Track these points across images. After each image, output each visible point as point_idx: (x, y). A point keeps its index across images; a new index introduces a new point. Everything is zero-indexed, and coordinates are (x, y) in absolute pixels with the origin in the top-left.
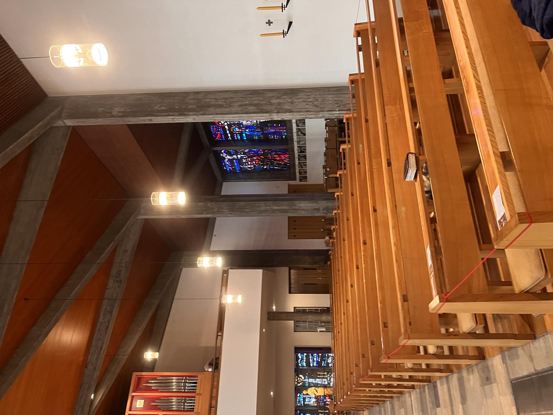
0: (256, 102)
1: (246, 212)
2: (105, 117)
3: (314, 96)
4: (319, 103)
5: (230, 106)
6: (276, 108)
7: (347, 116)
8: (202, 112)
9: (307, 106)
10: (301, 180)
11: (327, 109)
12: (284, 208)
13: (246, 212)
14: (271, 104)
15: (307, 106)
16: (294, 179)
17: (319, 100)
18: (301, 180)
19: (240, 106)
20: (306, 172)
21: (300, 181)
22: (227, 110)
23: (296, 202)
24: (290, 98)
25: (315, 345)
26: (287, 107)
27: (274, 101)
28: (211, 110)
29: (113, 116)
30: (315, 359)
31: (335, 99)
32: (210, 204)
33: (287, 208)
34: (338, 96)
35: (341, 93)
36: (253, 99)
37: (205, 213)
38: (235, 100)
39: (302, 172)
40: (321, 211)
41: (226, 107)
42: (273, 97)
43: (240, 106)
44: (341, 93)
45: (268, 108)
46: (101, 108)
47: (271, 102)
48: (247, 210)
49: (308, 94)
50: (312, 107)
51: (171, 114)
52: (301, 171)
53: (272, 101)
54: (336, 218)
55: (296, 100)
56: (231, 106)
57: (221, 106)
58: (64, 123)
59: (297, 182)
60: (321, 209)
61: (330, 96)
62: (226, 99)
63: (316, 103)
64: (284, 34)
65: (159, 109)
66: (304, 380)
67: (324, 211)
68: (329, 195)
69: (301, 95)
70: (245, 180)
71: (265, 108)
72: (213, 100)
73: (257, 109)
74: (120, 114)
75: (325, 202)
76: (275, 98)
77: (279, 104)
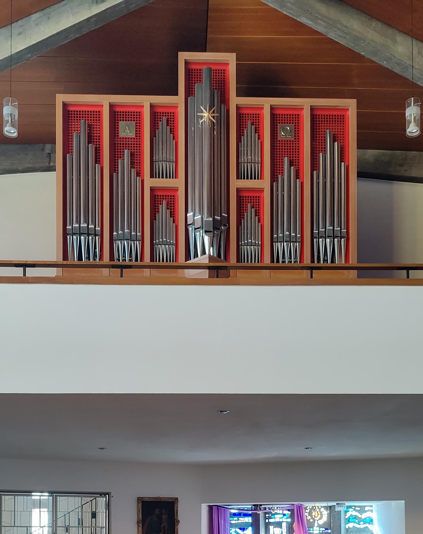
66: (316, 525)
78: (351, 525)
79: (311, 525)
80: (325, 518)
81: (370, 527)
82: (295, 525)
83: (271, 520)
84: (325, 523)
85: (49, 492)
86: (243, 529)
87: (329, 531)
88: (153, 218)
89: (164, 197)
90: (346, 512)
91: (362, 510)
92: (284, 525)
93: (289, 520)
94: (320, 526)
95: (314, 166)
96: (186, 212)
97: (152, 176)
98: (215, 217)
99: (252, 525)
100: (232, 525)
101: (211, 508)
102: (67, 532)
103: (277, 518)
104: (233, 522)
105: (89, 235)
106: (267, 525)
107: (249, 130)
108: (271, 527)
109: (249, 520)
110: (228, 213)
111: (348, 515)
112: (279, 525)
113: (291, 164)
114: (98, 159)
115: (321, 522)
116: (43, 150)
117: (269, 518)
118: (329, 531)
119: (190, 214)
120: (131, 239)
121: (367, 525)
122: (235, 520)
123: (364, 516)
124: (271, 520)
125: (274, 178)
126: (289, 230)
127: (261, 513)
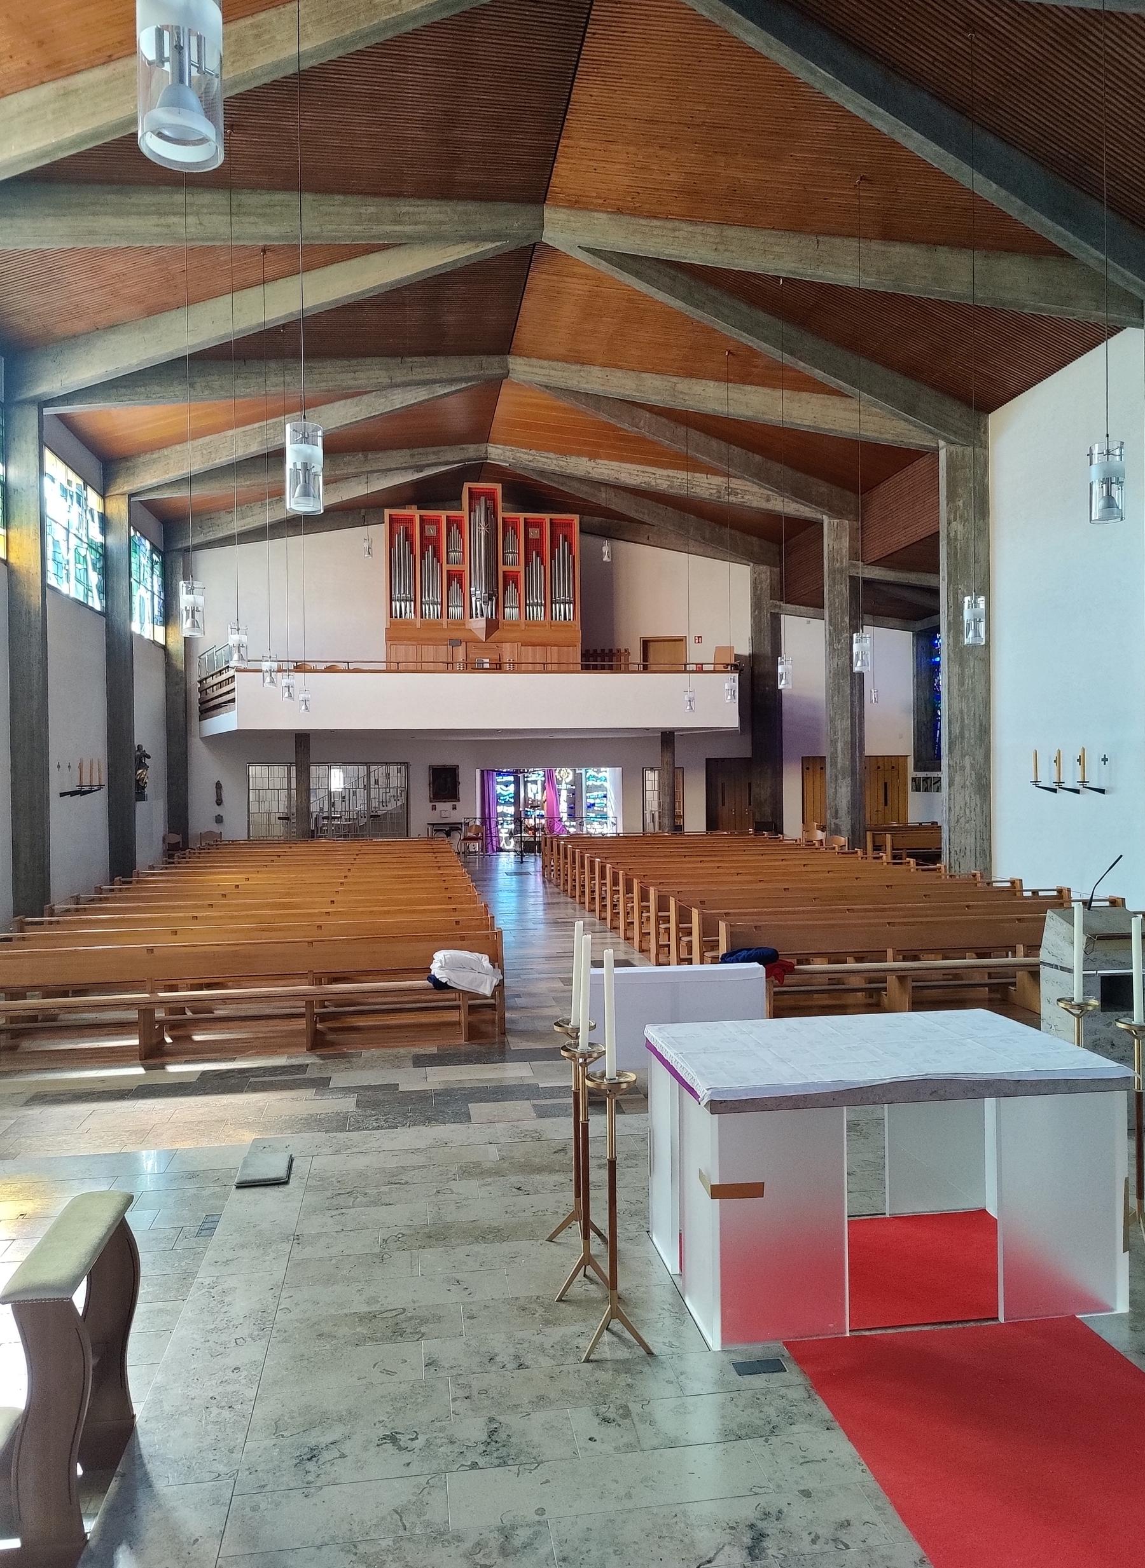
0: (967, 734)
1: (833, 697)
2: (949, 513)
3: (974, 818)
4: (963, 826)
5: (962, 696)
6: (956, 763)
7: (943, 868)
8: (952, 655)
9: (957, 808)
10: (914, 779)
11: (952, 837)
12: (839, 760)
13: (833, 697)
14: (963, 756)
15: (957, 808)
16: (916, 769)
17: (967, 825)
18: (914, 779)
19: (961, 711)
20: (926, 790)
21: (913, 778)
22: (955, 693)
23: (848, 780)
24: (972, 784)
25: (426, 271)
26: (957, 779)
27: (967, 761)
28: (956, 669)
29: (949, 524)
30: (598, 801)
31: (968, 848)
32: (847, 637)
33: (839, 765)
34: (973, 852)
35: (978, 855)
36: (972, 729)
37: (831, 628)
38: (972, 704)
39: (927, 783)
40: (834, 821)
41: (959, 691)
42: (974, 759)
43: (961, 711)
44: (978, 855)
45: (957, 752)
46: (964, 503)
47: (965, 756)
48: (836, 698)
49: (978, 809)
50: (956, 815)
51: (951, 610)
52: (929, 781)
53: (967, 757)
54: (131, 882)
55: (967, 793)
56: (961, 698)
57: (961, 683)
58: (943, 448)
59: (911, 773)
60: (837, 821)
61: (973, 840)
62: (973, 690)
63: (962, 820)
64: (1036, 783)
65: (959, 591)
66: (564, 782)
67: (833, 826)
68: (862, 834)
69: (976, 800)
70: (918, 675)
71: (957, 747)
72: (972, 671)
73: (956, 737)
74: (952, 534)
75: (849, 827)
76: (973, 762)
77: (963, 768)
78: (590, 783)
79: (559, 783)
80: (571, 777)
81: (605, 784)
82: (546, 784)
83: (529, 779)
84: (570, 781)
85: (151, 543)
86: (507, 786)
87: (574, 787)
88: (448, 589)
89: (455, 576)
90: (586, 772)
91: (598, 772)
92: (539, 783)
93: (543, 779)
94: (567, 784)
95: (553, 557)
96: (470, 587)
97: (447, 563)
98: (507, 1015)
99: (514, 782)
100: (498, 783)
101: (482, 772)
102: (990, 978)
103: (533, 777)
104: (498, 780)
105: (406, 600)
106: (526, 783)
107: (511, 532)
108: (529, 784)
109: (511, 778)
110: (498, 588)
111: (588, 775)
112: (535, 782)
113: (537, 555)
114: (412, 551)
115: (568, 780)
116: (360, 513)
117: (527, 777)
118: (574, 787)
119: (472, 589)
120: (434, 603)
121: (602, 782)
122: (499, 779)
123: (600, 775)
124: (529, 779)
125: (527, 565)
126: (537, 598)
127: (521, 775)
